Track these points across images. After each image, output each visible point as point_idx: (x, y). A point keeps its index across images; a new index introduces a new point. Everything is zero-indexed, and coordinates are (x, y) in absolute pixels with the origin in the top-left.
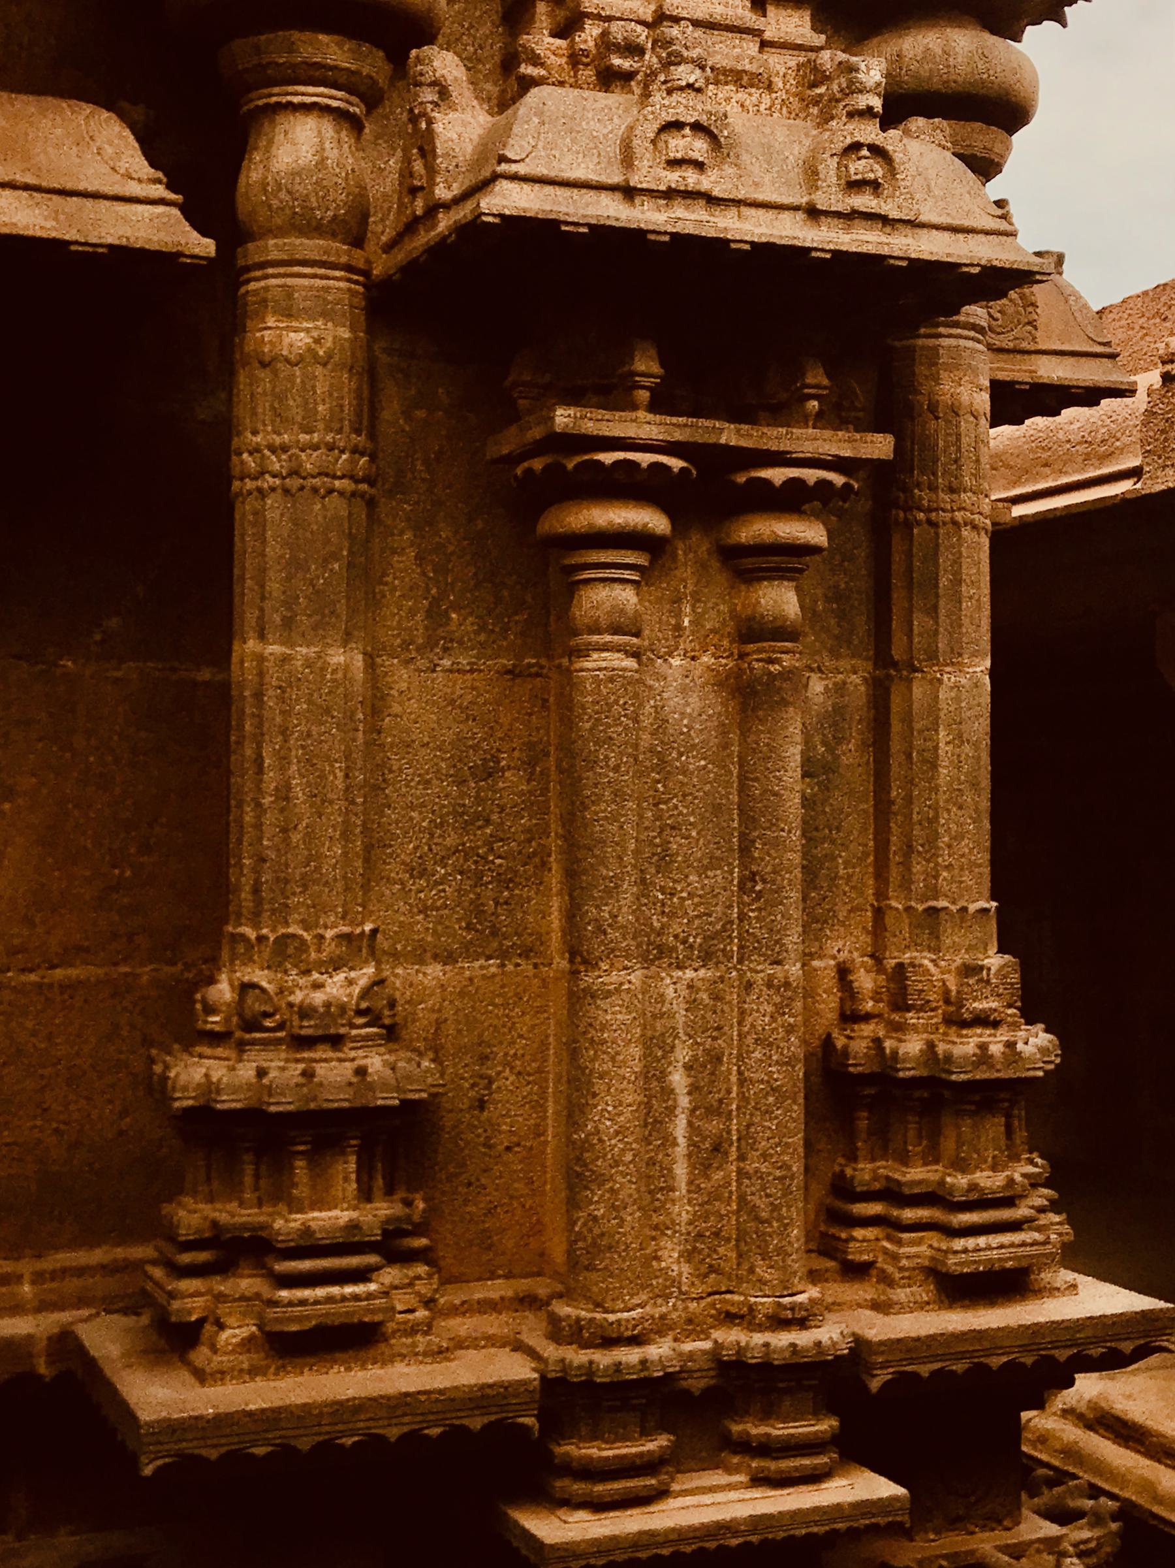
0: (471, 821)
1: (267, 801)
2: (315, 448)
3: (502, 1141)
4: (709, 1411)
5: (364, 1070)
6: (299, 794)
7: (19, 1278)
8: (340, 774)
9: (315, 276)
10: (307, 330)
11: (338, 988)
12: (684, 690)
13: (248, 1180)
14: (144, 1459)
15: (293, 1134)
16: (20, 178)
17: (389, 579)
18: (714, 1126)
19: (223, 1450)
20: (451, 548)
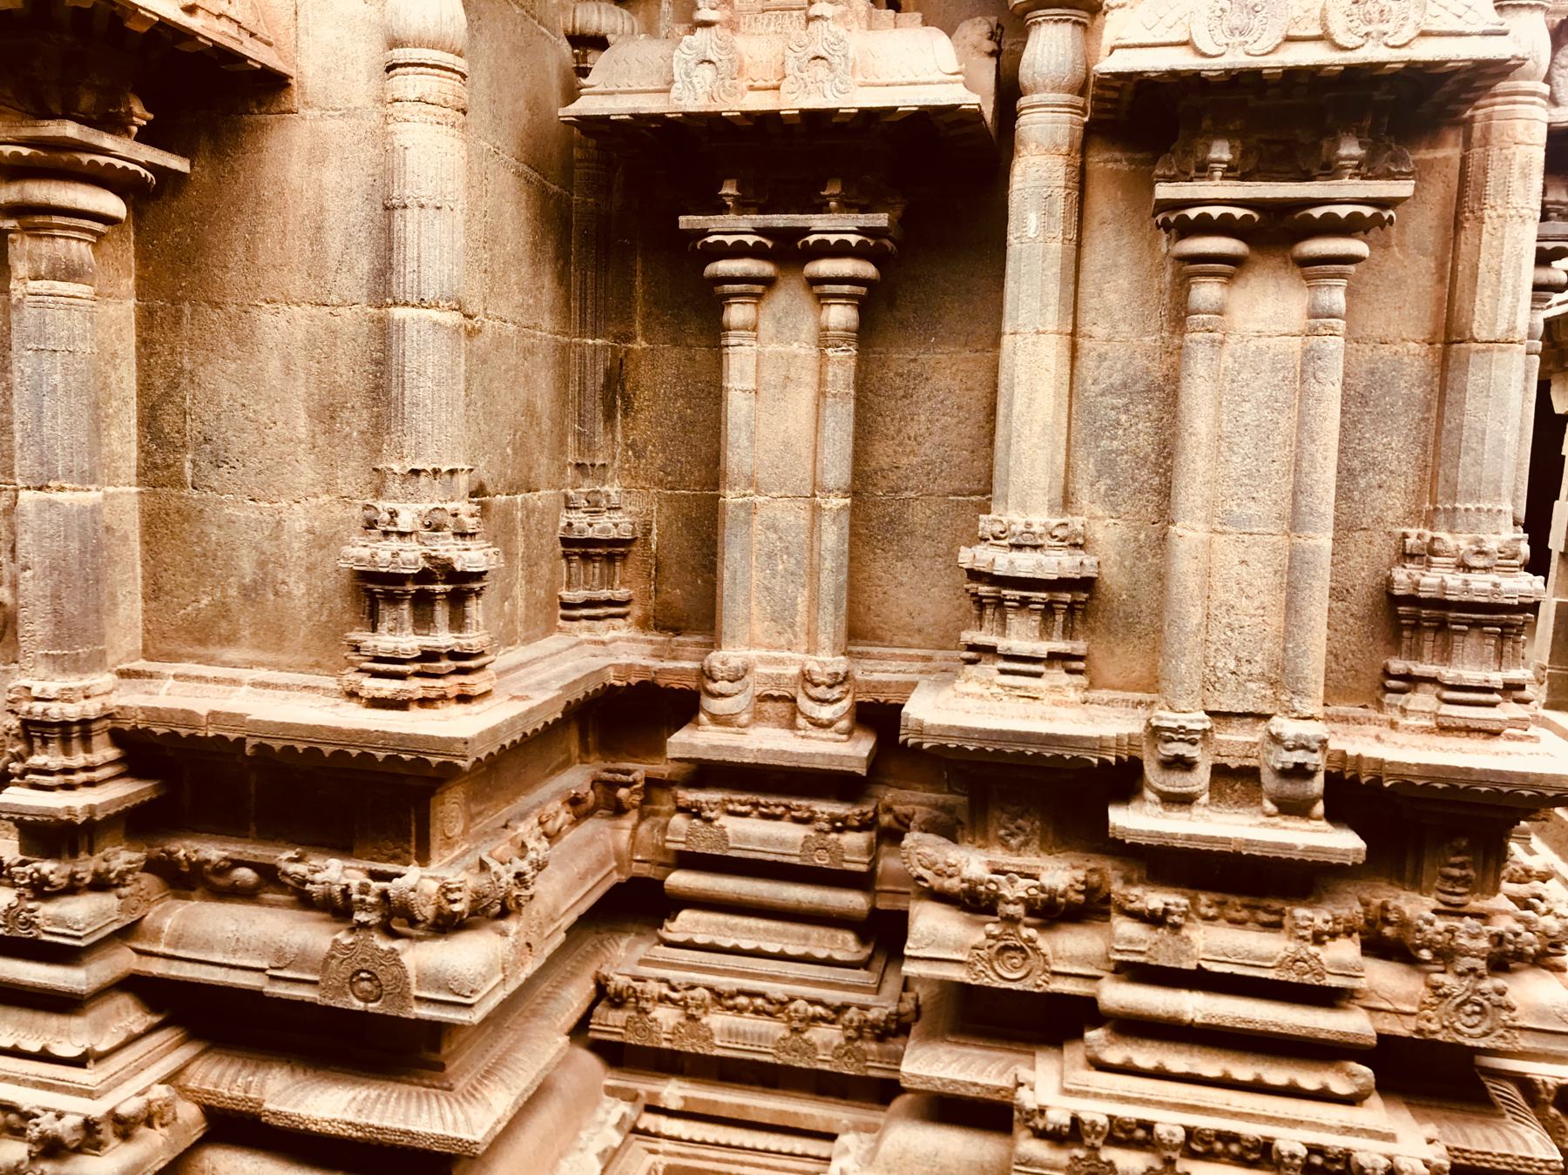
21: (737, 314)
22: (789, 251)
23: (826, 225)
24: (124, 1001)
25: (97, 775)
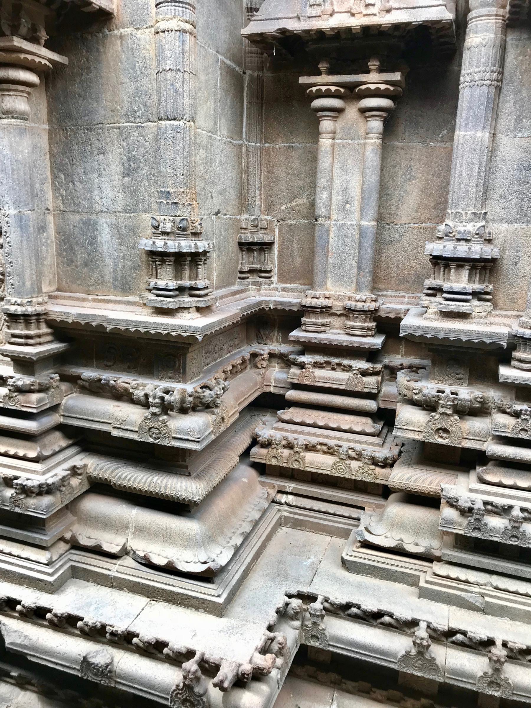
0: (521, 182)
1: (457, 176)
2: (479, 72)
3: (521, 274)
5: (477, 250)
6: (464, 174)
7: (405, 297)
8: (477, 168)
9: (485, 20)
10: (481, 37)
11: (471, 227)
13: (441, 274)
14: (401, 333)
15: (450, 263)
16: (402, 6)
17: (504, 110)
19: (420, 334)
20: (526, 99)
21: (326, 125)
22: (352, 93)
23: (373, 79)
24: (58, 435)
25: (42, 340)
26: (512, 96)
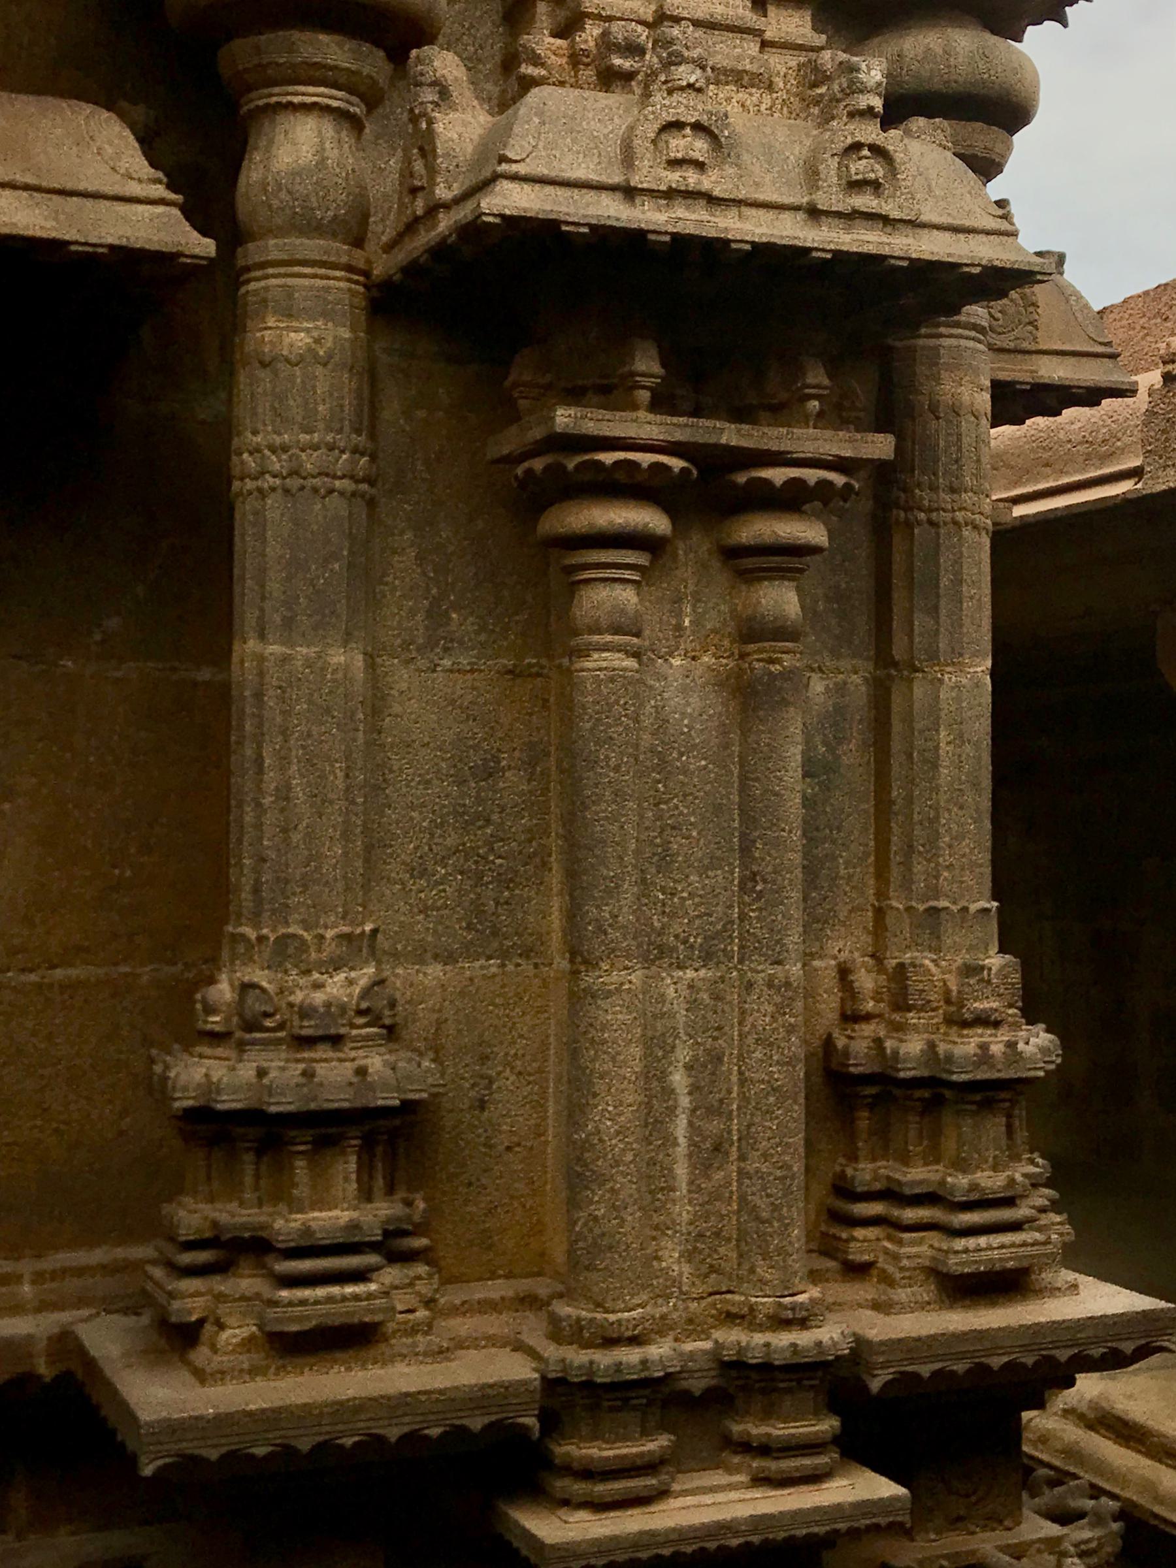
1: (267, 801)
2: (315, 447)
3: (502, 1141)
4: (710, 1409)
5: (363, 1072)
8: (340, 774)
10: (308, 330)
11: (339, 987)
12: (684, 690)
13: (248, 1180)
14: (143, 1459)
16: (20, 178)
17: (390, 579)
18: (714, 1126)
19: (224, 1450)
20: (451, 549)
26: (408, 535)
